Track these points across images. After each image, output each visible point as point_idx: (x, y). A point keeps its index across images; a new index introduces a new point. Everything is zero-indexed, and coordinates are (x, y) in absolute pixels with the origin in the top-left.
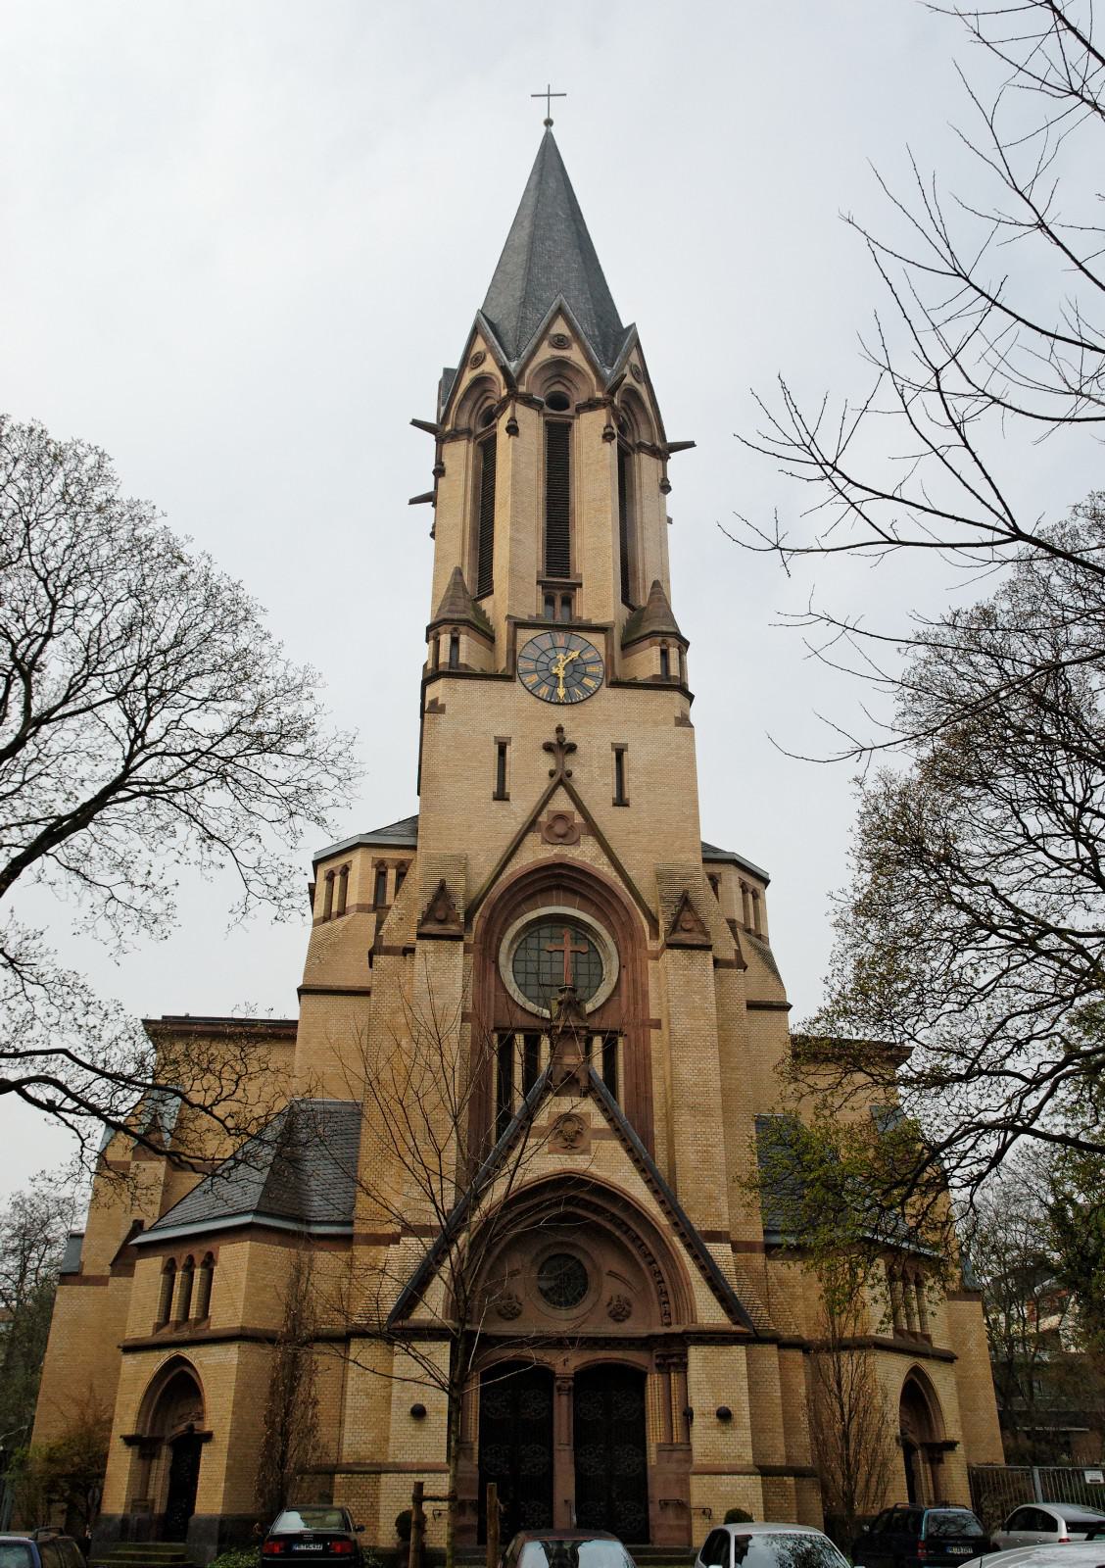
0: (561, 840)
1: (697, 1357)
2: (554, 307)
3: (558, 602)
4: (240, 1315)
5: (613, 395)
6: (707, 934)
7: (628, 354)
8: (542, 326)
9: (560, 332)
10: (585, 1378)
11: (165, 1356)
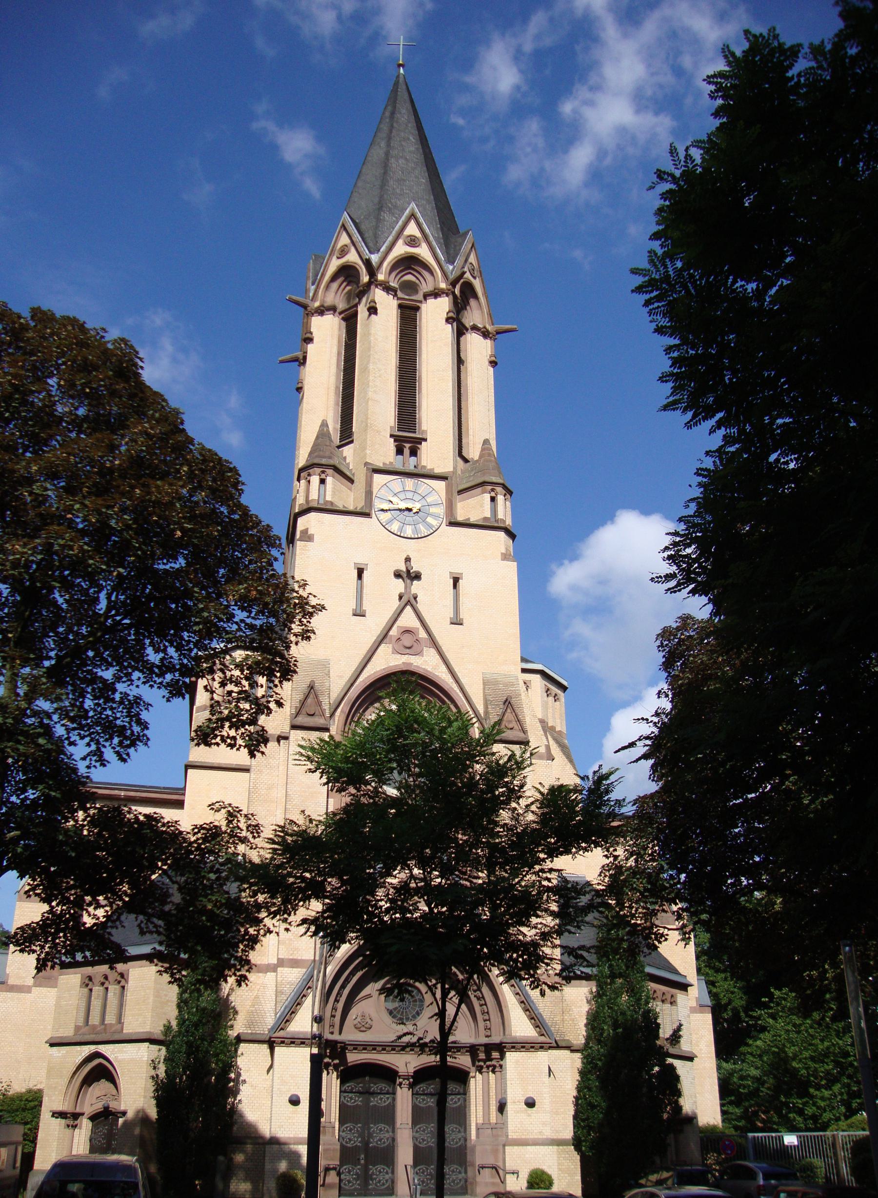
0: (408, 651)
1: (512, 1058)
2: (407, 212)
3: (407, 451)
4: (149, 1023)
5: (454, 287)
6: (524, 732)
8: (397, 228)
9: (412, 233)
10: (421, 1076)
11: (87, 1050)
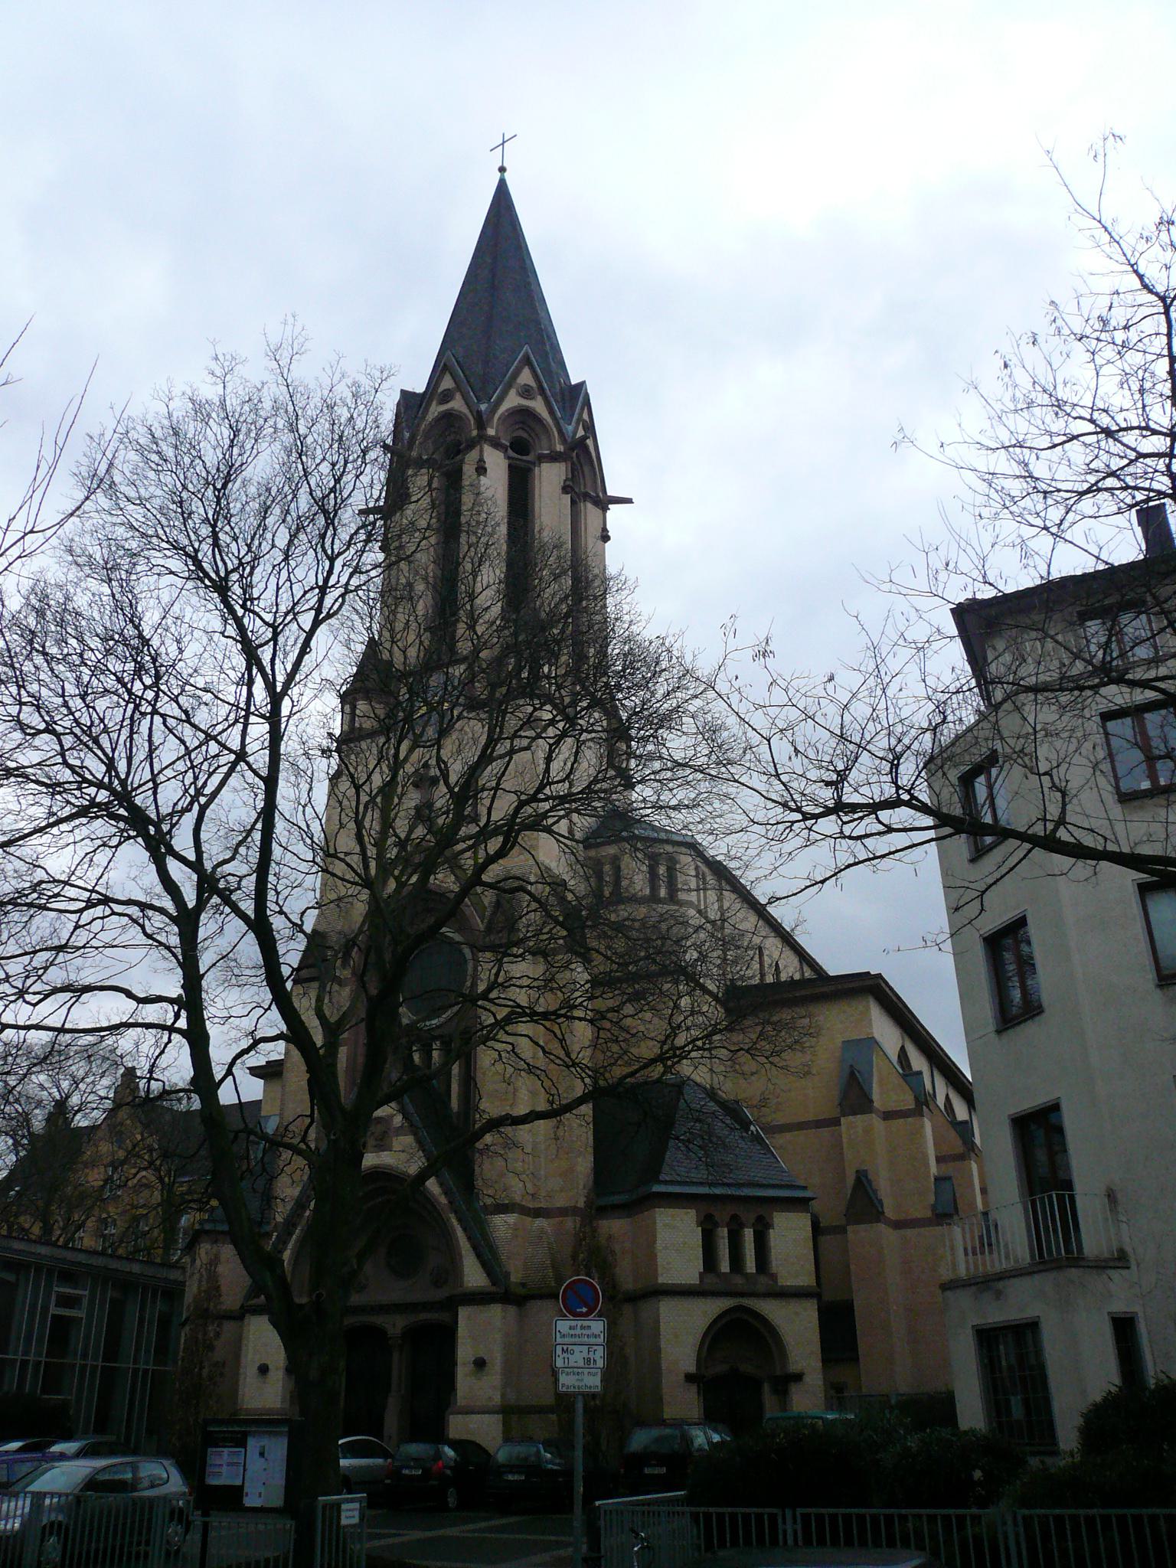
7: (581, 414)
